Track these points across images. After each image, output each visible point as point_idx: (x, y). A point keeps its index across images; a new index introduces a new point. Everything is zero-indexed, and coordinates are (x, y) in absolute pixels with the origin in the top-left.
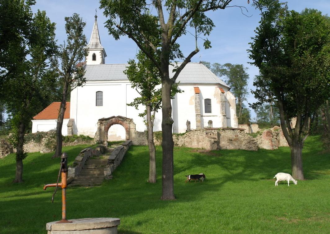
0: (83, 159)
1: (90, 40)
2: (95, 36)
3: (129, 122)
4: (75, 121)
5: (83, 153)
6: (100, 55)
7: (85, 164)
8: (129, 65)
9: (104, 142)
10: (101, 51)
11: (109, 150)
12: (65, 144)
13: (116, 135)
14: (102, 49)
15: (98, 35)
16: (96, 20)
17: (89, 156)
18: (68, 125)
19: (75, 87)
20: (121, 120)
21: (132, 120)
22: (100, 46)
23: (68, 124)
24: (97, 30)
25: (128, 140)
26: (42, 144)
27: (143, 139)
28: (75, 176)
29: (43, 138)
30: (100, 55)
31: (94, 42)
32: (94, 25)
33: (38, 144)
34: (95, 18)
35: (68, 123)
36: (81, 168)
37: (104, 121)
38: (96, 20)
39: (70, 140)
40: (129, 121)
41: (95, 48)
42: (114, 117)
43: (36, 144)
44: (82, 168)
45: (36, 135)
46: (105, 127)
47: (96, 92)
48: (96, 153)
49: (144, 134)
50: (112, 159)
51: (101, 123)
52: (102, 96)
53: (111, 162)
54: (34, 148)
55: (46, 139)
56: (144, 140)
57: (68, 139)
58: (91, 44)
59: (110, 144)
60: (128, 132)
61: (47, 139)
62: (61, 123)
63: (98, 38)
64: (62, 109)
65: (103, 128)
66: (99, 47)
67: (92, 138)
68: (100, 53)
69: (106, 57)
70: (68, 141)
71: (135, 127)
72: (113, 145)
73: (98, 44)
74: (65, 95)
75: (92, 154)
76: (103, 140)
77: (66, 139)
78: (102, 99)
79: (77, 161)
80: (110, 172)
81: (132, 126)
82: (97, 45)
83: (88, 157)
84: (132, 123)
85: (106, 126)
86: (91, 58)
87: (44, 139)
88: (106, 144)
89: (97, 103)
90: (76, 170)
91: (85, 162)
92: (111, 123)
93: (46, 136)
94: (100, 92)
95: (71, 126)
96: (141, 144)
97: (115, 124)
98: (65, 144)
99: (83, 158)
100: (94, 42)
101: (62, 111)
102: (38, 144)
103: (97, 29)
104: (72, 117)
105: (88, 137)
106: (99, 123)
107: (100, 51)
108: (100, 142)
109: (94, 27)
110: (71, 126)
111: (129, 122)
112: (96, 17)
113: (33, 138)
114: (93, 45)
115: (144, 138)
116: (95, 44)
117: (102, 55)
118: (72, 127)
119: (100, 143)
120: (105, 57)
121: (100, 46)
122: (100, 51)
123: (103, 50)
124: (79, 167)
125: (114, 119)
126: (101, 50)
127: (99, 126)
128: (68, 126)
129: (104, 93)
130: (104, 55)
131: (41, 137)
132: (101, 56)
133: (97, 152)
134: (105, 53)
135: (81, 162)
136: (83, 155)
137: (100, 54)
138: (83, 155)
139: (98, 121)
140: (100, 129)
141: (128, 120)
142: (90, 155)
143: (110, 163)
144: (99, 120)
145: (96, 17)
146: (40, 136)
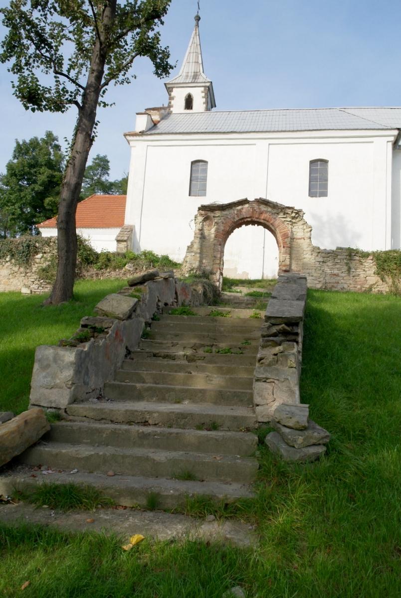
0: (134, 309)
1: (182, 67)
2: (192, 58)
3: (293, 218)
4: (137, 229)
5: (139, 287)
6: (203, 97)
7: (145, 335)
8: (73, 532)
9: (212, 273)
10: (205, 89)
11: (226, 297)
12: (97, 275)
13: (236, 269)
14: (208, 84)
15: (200, 56)
16: (197, 25)
17: (166, 304)
18: (119, 238)
19: (130, 58)
20: (267, 212)
21: (301, 214)
22: (203, 78)
23: (118, 236)
24: (199, 46)
25: (286, 271)
26: (34, 269)
27: (336, 272)
28: (74, 400)
29: (37, 253)
30: (203, 97)
31: (190, 71)
32: (192, 36)
33: (22, 269)
34: (195, 22)
35: (120, 234)
36: (123, 352)
37: (218, 213)
38: (197, 25)
39: (113, 264)
40: (293, 215)
41: (191, 83)
42: (245, 202)
43: (16, 269)
44: (129, 352)
45: (19, 244)
46: (217, 231)
47: (193, 163)
48: (190, 297)
49: (339, 257)
50: (287, 315)
51: (206, 219)
52: (205, 171)
53: (284, 333)
54: (11, 280)
55: (45, 255)
56: (337, 275)
57: (109, 260)
58: (184, 74)
59: (229, 283)
60: (289, 245)
61: (48, 256)
62: (72, 187)
63: (200, 62)
64: (81, 137)
65: (211, 232)
66: (201, 80)
67: (178, 262)
68: (202, 92)
69: (214, 108)
70: (107, 266)
71: (309, 234)
72: (237, 285)
73: (198, 74)
74: (93, 89)
75: (177, 298)
76: (208, 268)
77: (102, 260)
78: (205, 179)
79: (106, 314)
80: (292, 392)
81: (299, 231)
82: (196, 76)
83: (161, 304)
84: (301, 222)
85: (222, 228)
86: (183, 103)
87: (40, 256)
88: (219, 281)
89: (192, 189)
90: (81, 366)
91: (148, 324)
92: (237, 219)
93: (47, 249)
94: (201, 163)
95: (125, 241)
96: (329, 286)
97: (247, 223)
98: (97, 275)
99: (136, 305)
100: (190, 71)
101: (79, 147)
102: (22, 269)
103: (198, 43)
104: (128, 221)
105: (166, 258)
106: (200, 219)
107: (203, 89)
108: (201, 273)
109: (192, 39)
110: (125, 241)
111: (293, 218)
112: (198, 19)
113: (10, 251)
114: (187, 76)
115: (339, 269)
116: (193, 74)
117: (206, 97)
118: (129, 242)
119: (200, 277)
120: (212, 107)
121: (203, 78)
122: (203, 89)
123: (208, 87)
124: (106, 346)
125: (247, 206)
126: (202, 86)
127: (199, 226)
128: (118, 241)
130: (211, 98)
131: (32, 249)
132: (204, 100)
133: (193, 295)
134: (213, 100)
135: (127, 322)
136: (138, 294)
137: (203, 94)
138: (138, 294)
139: (196, 212)
140: (202, 236)
141: (289, 211)
142: (171, 300)
143: (275, 335)
144: (199, 209)
145: (198, 19)
146: (28, 246)
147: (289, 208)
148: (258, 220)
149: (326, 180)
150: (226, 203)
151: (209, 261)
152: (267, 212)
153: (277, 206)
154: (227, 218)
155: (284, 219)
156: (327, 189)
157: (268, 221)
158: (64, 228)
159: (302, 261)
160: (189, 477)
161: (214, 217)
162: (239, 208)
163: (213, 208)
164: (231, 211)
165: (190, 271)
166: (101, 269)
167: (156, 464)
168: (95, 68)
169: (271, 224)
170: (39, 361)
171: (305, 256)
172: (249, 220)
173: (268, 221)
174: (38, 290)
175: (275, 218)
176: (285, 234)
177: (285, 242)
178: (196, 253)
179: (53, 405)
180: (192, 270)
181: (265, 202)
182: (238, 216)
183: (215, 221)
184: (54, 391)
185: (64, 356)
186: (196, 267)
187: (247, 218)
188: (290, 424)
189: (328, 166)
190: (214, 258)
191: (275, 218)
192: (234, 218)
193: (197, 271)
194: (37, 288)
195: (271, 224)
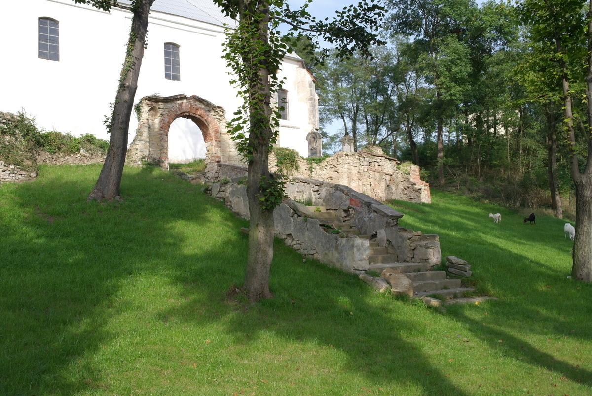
20: (201, 109)
37: (161, 105)
97: (184, 117)
125: (185, 101)
129: (62, 28)
141: (218, 110)
147: (218, 107)
148: (194, 115)
149: (178, 64)
150: (164, 96)
151: (155, 149)
152: (201, 109)
153: (211, 105)
154: (171, 110)
155: (214, 117)
156: (179, 73)
157: (202, 117)
158: (124, 128)
159: (227, 153)
160: (446, 288)
161: (159, 108)
162: (179, 102)
163: (158, 100)
164: (173, 104)
165: (143, 158)
166: (55, 153)
167: (436, 285)
168: (580, 192)
169: (205, 120)
170: (356, 247)
171: (231, 150)
172: (187, 114)
173: (202, 117)
174: (10, 177)
175: (208, 115)
176: (216, 129)
177: (217, 137)
178: (146, 142)
179: (363, 269)
180: (144, 157)
181: (201, 101)
182: (179, 110)
183: (161, 112)
184: (363, 261)
185: (365, 243)
186: (147, 155)
187: (186, 112)
188: (462, 263)
189: (179, 51)
190: (161, 148)
191: (208, 115)
192: (176, 112)
193: (148, 159)
194: (8, 175)
195: (205, 120)
